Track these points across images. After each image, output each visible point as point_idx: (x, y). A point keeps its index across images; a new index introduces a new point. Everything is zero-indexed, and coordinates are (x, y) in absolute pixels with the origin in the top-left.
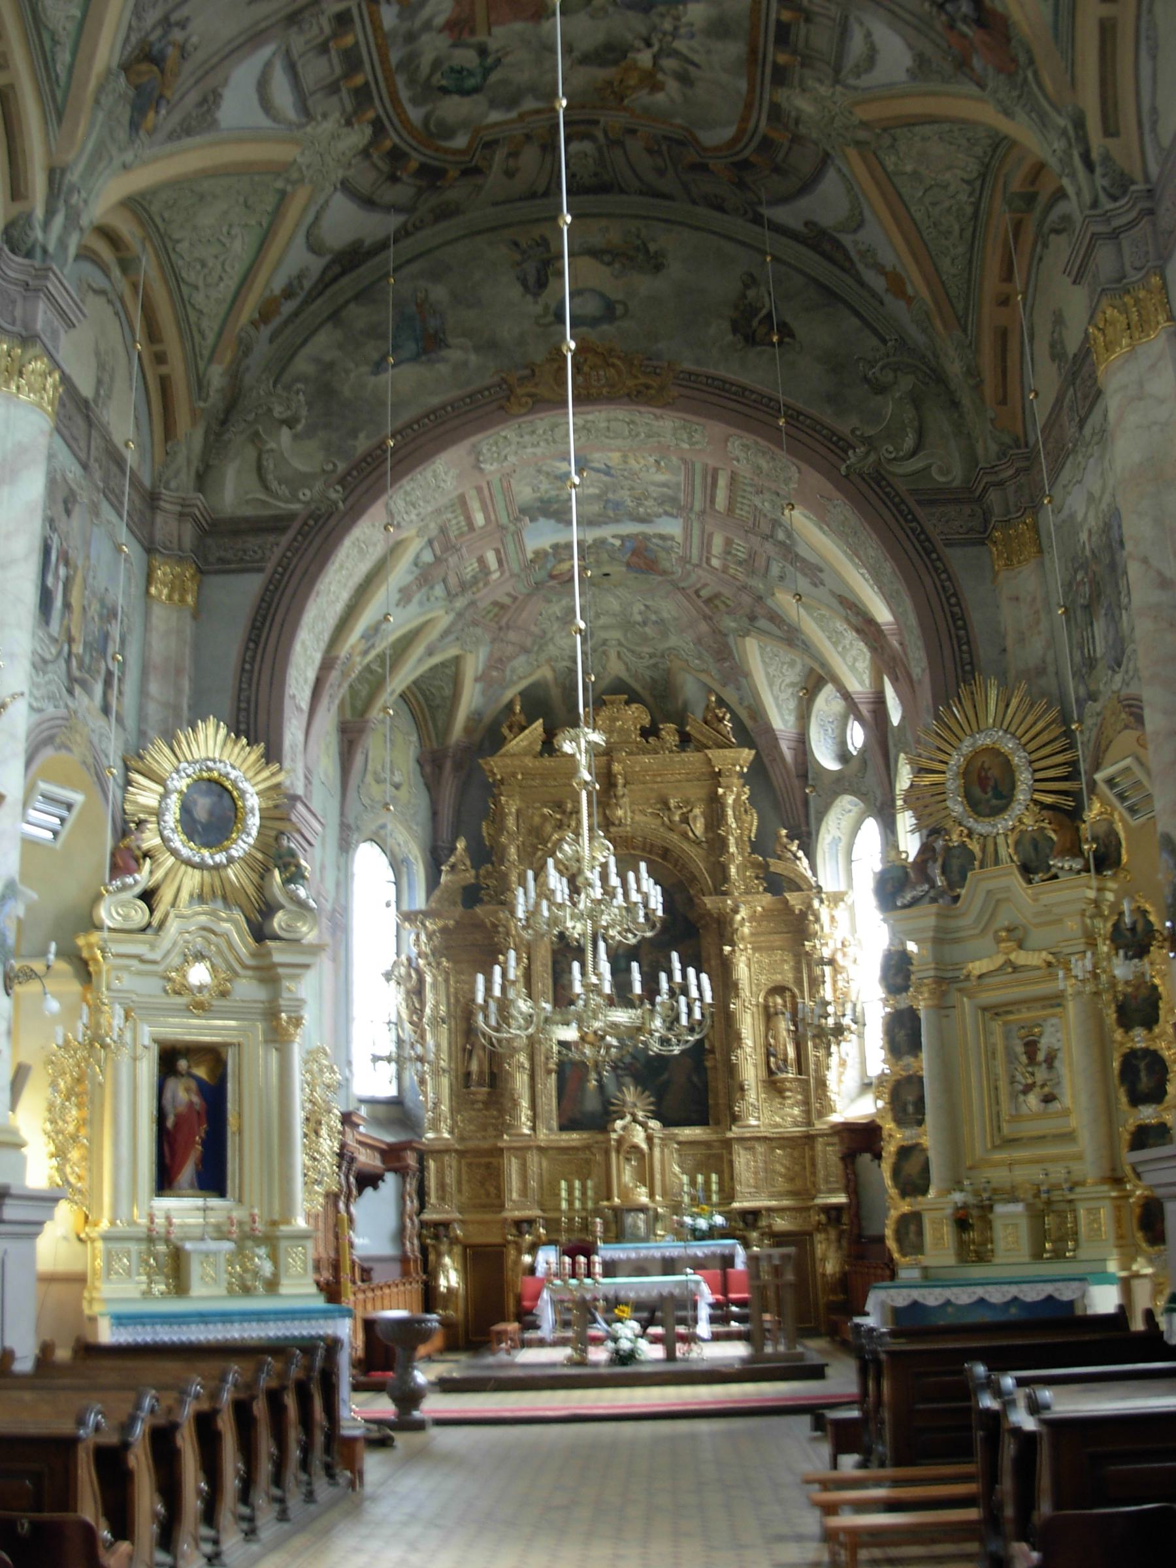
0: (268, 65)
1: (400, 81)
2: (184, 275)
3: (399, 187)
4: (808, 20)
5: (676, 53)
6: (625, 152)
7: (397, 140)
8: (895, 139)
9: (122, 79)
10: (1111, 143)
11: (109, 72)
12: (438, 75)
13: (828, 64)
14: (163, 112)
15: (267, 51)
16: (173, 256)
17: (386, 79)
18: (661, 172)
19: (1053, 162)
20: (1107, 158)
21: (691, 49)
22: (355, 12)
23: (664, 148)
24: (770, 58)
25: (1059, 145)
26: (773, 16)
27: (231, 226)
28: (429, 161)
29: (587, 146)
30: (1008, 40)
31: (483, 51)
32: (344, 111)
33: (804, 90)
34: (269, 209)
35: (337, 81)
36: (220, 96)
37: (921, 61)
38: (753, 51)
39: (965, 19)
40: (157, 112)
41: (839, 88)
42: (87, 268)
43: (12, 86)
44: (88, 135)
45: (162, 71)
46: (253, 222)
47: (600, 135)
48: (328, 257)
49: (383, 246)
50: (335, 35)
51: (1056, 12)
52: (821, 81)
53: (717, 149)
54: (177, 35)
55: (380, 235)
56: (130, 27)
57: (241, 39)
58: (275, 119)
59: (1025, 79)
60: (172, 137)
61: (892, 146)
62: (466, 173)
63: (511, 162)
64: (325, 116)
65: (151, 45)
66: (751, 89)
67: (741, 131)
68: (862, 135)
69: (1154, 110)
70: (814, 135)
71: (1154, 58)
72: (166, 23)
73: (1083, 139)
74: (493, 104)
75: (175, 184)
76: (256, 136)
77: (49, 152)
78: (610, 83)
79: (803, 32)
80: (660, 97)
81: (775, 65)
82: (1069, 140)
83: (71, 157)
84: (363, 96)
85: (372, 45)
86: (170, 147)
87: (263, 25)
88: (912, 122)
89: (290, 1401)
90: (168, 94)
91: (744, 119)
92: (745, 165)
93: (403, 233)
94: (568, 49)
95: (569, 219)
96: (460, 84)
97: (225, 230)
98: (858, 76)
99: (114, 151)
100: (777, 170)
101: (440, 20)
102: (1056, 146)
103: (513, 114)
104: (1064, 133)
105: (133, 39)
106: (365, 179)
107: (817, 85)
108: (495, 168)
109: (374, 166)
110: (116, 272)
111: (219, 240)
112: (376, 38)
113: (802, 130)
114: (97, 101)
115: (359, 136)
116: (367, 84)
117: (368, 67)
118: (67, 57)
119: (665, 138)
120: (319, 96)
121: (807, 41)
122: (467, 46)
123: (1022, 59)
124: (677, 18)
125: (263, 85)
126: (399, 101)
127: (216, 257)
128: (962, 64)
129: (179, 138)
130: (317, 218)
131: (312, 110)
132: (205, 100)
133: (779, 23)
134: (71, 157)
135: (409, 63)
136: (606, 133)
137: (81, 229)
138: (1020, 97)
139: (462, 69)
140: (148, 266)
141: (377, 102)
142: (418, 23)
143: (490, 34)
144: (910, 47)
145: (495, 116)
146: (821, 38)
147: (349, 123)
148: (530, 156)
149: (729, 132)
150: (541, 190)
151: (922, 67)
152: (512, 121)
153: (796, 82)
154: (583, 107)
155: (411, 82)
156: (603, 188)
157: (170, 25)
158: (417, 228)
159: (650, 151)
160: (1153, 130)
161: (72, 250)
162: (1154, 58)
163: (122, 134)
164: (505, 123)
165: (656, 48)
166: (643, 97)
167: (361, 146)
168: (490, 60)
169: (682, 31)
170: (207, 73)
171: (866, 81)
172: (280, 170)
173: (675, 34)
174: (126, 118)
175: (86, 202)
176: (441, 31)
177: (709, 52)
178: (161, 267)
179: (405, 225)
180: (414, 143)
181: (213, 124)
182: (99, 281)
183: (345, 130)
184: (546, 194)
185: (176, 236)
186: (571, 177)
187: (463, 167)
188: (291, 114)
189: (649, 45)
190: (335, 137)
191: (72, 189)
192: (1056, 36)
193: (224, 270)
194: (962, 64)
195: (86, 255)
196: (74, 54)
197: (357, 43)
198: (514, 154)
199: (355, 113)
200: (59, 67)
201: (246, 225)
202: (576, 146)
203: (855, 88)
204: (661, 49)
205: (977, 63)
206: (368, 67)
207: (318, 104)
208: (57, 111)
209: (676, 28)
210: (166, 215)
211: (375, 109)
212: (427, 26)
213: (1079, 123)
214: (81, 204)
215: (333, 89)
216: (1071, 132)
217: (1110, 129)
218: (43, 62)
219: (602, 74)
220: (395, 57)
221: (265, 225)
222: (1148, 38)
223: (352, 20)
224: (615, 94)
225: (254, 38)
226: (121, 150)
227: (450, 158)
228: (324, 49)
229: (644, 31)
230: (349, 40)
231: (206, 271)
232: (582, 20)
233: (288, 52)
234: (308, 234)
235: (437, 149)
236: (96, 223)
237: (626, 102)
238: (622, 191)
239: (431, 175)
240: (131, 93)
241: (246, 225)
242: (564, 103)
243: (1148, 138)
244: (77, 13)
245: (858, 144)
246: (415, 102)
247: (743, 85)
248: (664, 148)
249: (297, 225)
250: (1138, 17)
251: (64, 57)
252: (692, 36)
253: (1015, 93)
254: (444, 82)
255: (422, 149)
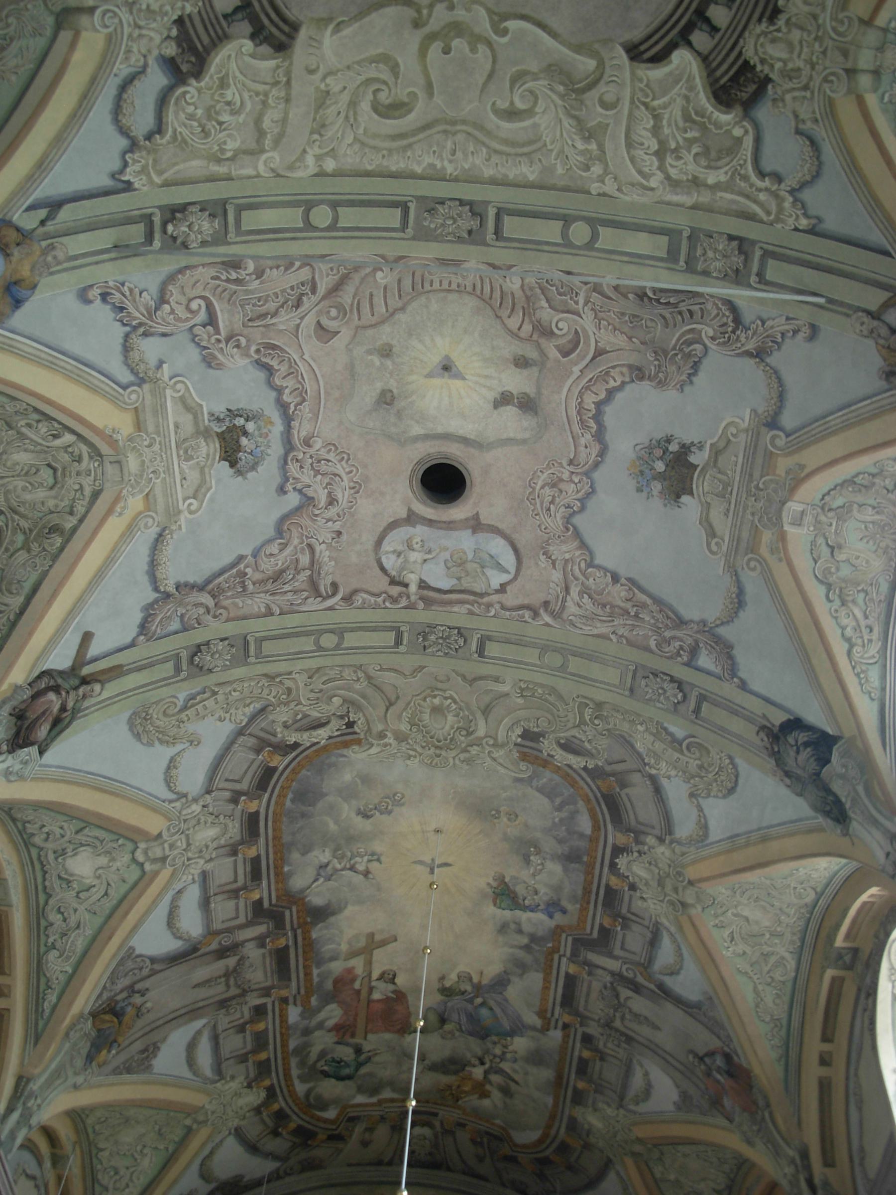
0: (199, 1033)
1: (294, 1062)
2: (100, 1176)
3: (278, 1140)
4: (602, 1059)
5: (500, 1071)
6: (455, 1140)
7: (283, 1105)
8: (662, 1154)
9: (90, 1022)
10: (827, 1170)
11: (81, 1015)
12: (322, 1062)
13: (615, 1092)
14: (114, 1052)
15: (199, 1024)
16: (94, 1160)
17: (283, 1059)
18: (481, 1159)
19: (784, 1183)
20: (826, 1183)
21: (515, 1071)
22: (270, 1007)
23: (485, 1140)
24: (572, 1083)
25: (789, 1170)
26: (576, 1053)
27: (144, 1146)
28: (306, 1125)
29: (426, 1131)
30: (751, 1087)
31: (358, 1050)
32: (247, 1078)
33: (595, 1110)
34: (177, 1139)
35: (247, 1054)
36: (159, 1048)
37: (685, 1096)
38: (559, 1077)
39: (719, 1070)
40: (109, 1051)
41: (622, 1111)
42: (27, 1156)
43: (9, 987)
44: (52, 1059)
45: (120, 1023)
46: (162, 1147)
47: (437, 1124)
48: (213, 1186)
49: (258, 1183)
50: (251, 1021)
51: (786, 1070)
52: (609, 1105)
53: (524, 1146)
54: (137, 1000)
55: (258, 1174)
56: (105, 987)
57: (183, 1011)
58: (195, 1073)
59: (763, 1119)
60: (116, 1071)
61: (660, 1159)
62: (331, 1138)
63: (367, 1136)
64: (233, 1078)
65: (117, 1002)
66: (556, 1104)
67: (545, 1135)
68: (637, 1148)
69: (862, 1149)
70: (601, 1144)
71: (860, 1109)
72: (131, 990)
73: (808, 1167)
74: (360, 1090)
75: (108, 1106)
76: (177, 1083)
77: (22, 1064)
78: (450, 1087)
79: (597, 1068)
80: (486, 1102)
81: (575, 1088)
82: (796, 1166)
83: (37, 1071)
84: (264, 1068)
85: (278, 1035)
86: (112, 1079)
87: (201, 1004)
88: (676, 1142)
89: (286, 28)
90: (120, 1039)
91: (549, 1127)
92: (545, 1162)
93: (275, 1176)
94: (422, 1058)
95: (414, 1103)
96: (337, 1071)
97: (139, 1148)
98: (637, 1104)
99: (70, 1073)
100: (570, 1168)
101: (330, 1023)
102: (787, 1170)
103: (374, 1100)
104: (792, 1161)
105: (105, 996)
106: (254, 1131)
107: (605, 1107)
108: (354, 1137)
109: (263, 1122)
110: (48, 1164)
111: (133, 1156)
112: (281, 1027)
113: (592, 1140)
114: (67, 1035)
115: (255, 1097)
116: (268, 1059)
117: (271, 1047)
118: (54, 999)
119: (487, 1133)
120: (232, 1061)
121: (601, 1074)
122: (347, 1044)
123: (761, 1103)
124: (505, 1047)
125: (191, 1047)
126: (290, 1076)
127: (127, 1168)
128: (716, 1103)
129: (121, 1074)
130: (212, 1153)
131: (224, 1072)
132: (145, 1050)
133: (581, 1059)
134: (37, 1071)
135: (302, 1051)
136: (442, 1124)
137: (30, 1127)
138: (759, 1131)
139: (341, 1061)
140: (74, 1165)
141: (274, 1074)
142: (314, 1022)
143: (365, 1038)
144: (677, 1086)
145: (360, 1099)
146: (611, 1073)
147: (249, 1086)
148: (382, 1132)
149: (533, 1136)
150: (386, 1160)
151: (685, 1102)
152: (372, 1105)
153: (590, 1102)
154: (427, 1102)
155: (302, 1064)
156: (435, 1165)
157: (134, 992)
158: (287, 1174)
159: (474, 1142)
160: (862, 1164)
161: (19, 1141)
162: (860, 1109)
163: (79, 1062)
164: (366, 1105)
165: (487, 1066)
166: (473, 1101)
167: (255, 1104)
168: (363, 1057)
169: (508, 1056)
170: (152, 1030)
171: (643, 1108)
172: (191, 1111)
173: (502, 1058)
174: (84, 1052)
175: (39, 1106)
176: (329, 1031)
177: (526, 1074)
178: (83, 1167)
179: (278, 1169)
180: (296, 1109)
181: (149, 1068)
182: (33, 1169)
183: (246, 1090)
184: (390, 1163)
185: (101, 1146)
186: (411, 1152)
187: (330, 1133)
188: (208, 1072)
189: (482, 1063)
190: (237, 1094)
191: (32, 1095)
192: (787, 1089)
193: (131, 1180)
194: (716, 1103)
195: (29, 1146)
196: (59, 998)
197: (267, 1029)
198: (370, 1130)
199: (255, 1080)
200: (46, 1004)
201: (156, 1148)
202: (418, 1130)
203: (635, 1113)
204: (491, 1067)
205: (727, 1102)
206: (271, 1047)
207: (230, 1068)
208: (36, 1036)
209: (504, 1053)
210: (97, 1128)
211: (271, 1079)
212: (320, 1026)
213: (805, 1154)
214: (35, 1108)
215: (243, 1059)
216: (798, 1161)
217: (829, 1162)
218: (36, 998)
219: (445, 1080)
220: (292, 1044)
221: (170, 1151)
222: (855, 1094)
223: (266, 1013)
224: (451, 1096)
225: (192, 1012)
226: (76, 1074)
227: (322, 1125)
228: (241, 1029)
229: (480, 1053)
230: (261, 1026)
231: (118, 1177)
232: (435, 1039)
233: (215, 1027)
234: (201, 1165)
235: (312, 1116)
236: (42, 1124)
237: (460, 1102)
238: (449, 1169)
239: (304, 1136)
240: (94, 1034)
241: (156, 1148)
242: (422, 1023)
243: (857, 1169)
244: (70, 970)
245: (634, 1154)
246: (303, 1079)
247: (550, 1101)
248: (485, 1140)
249: (196, 1154)
250: (847, 1079)
251: (52, 998)
252: (515, 1061)
253: (755, 1128)
254: (326, 1068)
255: (302, 1115)
